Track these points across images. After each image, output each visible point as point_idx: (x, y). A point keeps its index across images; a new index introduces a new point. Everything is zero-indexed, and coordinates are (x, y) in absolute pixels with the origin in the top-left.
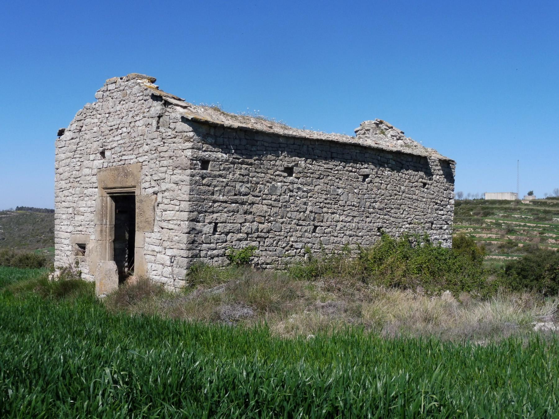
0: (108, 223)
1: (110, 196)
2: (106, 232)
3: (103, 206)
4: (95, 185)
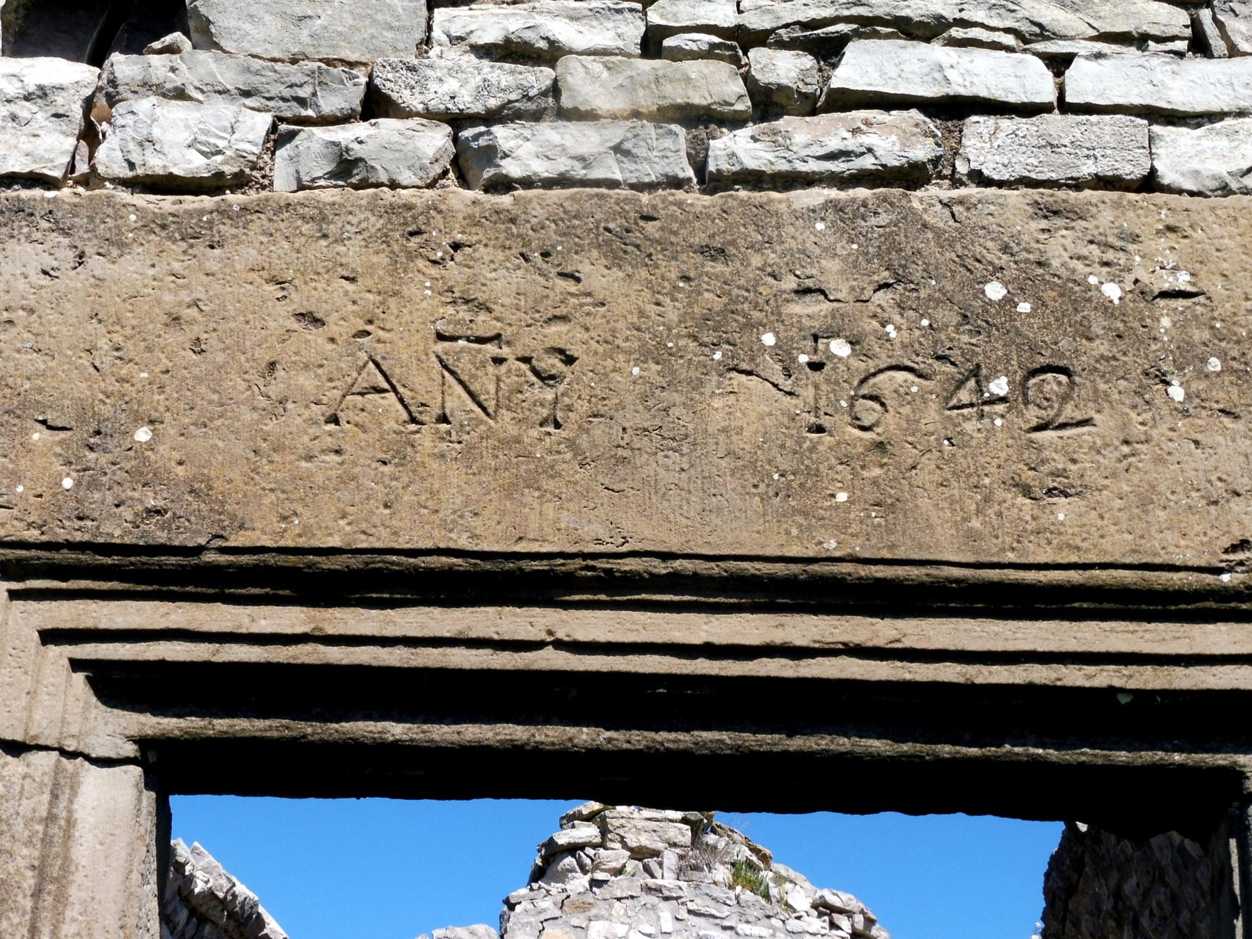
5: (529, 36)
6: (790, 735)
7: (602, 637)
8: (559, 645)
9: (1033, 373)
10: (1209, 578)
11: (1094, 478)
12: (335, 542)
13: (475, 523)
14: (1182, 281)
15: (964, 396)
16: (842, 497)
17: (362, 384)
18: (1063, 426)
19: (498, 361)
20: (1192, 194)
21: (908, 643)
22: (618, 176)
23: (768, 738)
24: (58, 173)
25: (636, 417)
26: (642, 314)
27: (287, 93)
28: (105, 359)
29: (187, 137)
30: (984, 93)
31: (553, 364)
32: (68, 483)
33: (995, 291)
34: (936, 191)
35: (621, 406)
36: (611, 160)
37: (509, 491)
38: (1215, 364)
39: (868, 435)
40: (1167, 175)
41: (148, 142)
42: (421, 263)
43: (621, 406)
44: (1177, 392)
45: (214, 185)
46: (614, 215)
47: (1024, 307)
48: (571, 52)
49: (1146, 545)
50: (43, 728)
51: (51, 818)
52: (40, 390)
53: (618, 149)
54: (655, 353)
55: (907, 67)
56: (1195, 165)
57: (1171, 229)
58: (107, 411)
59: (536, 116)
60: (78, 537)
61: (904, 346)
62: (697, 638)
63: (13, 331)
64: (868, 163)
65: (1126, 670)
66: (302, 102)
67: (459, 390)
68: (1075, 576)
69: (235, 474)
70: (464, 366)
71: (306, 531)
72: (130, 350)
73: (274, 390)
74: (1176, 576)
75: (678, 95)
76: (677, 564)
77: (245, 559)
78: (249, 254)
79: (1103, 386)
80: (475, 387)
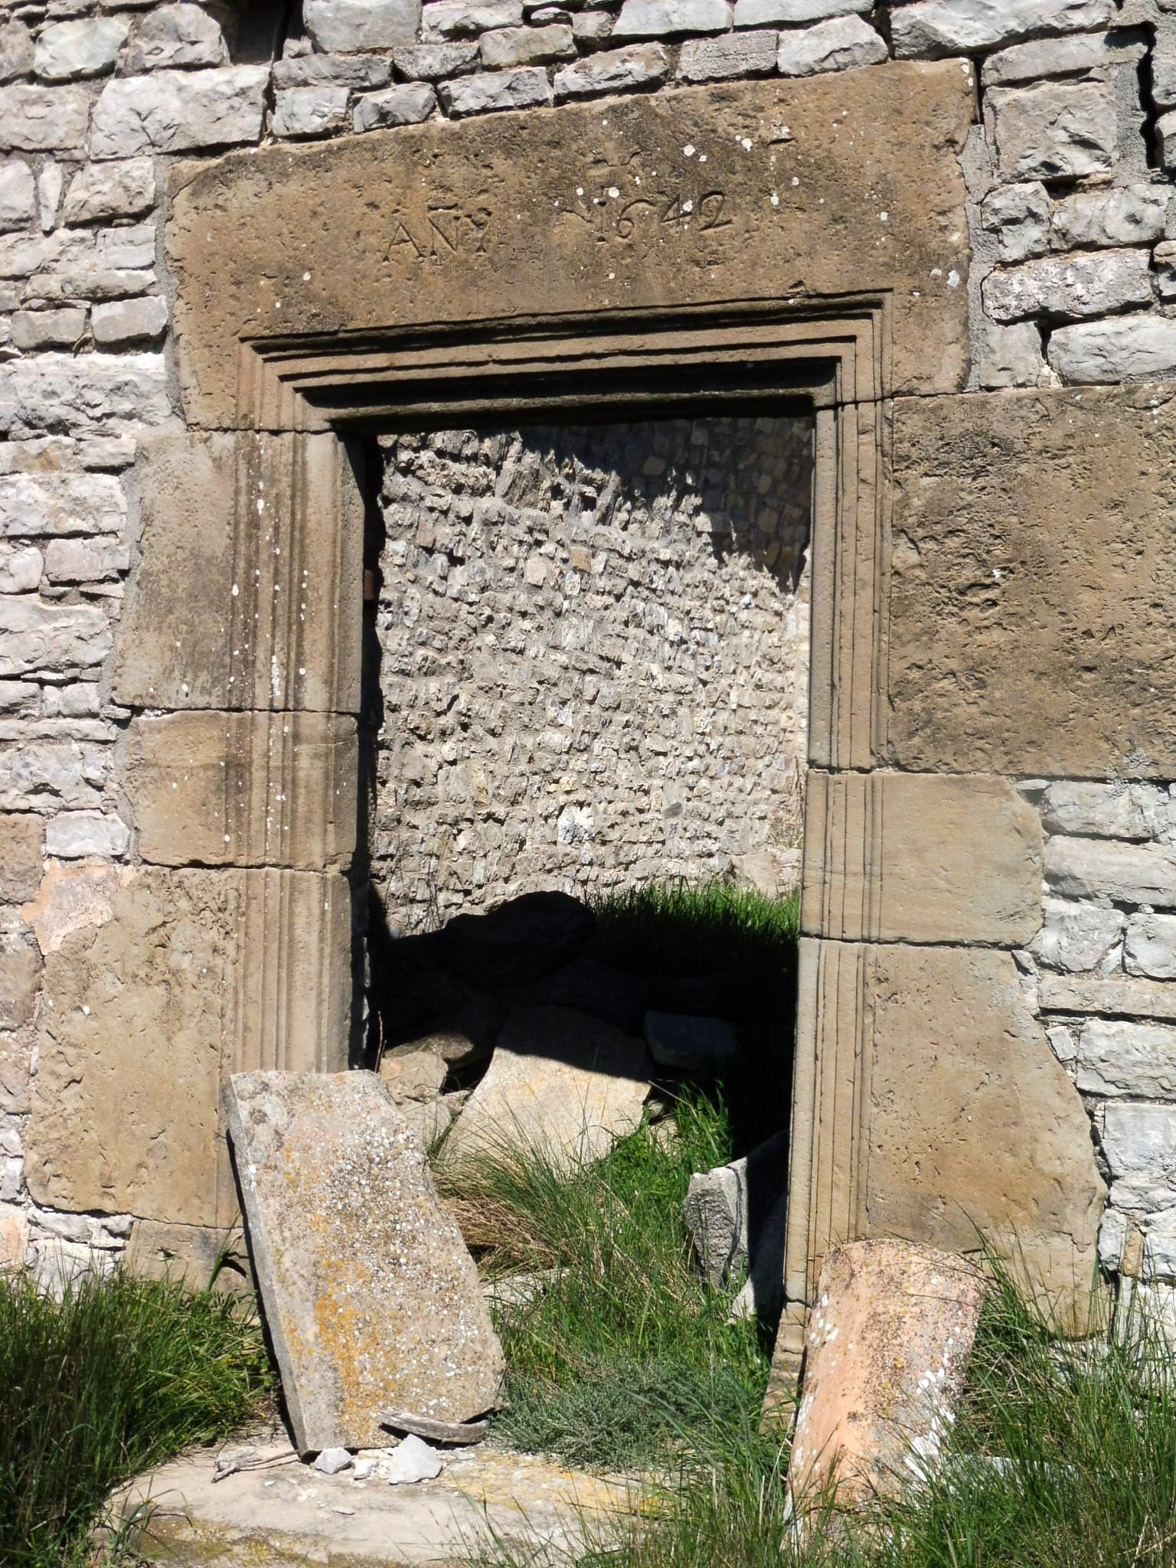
0: (315, 695)
1: (339, 427)
2: (291, 785)
3: (255, 523)
4: (147, 317)
5: (466, 22)
6: (604, 394)
7: (513, 356)
8: (495, 362)
9: (706, 196)
10: (782, 303)
11: (731, 253)
12: (391, 323)
13: (450, 306)
14: (784, 132)
15: (671, 214)
16: (612, 276)
17: (398, 238)
18: (718, 225)
19: (457, 218)
20: (797, 76)
21: (647, 347)
22: (511, 103)
23: (594, 396)
24: (255, 138)
25: (519, 243)
26: (521, 184)
27: (354, 75)
28: (287, 239)
29: (310, 109)
30: (690, 27)
31: (483, 216)
32: (278, 305)
33: (689, 150)
34: (667, 91)
35: (512, 237)
36: (507, 94)
37: (463, 289)
38: (796, 181)
39: (626, 241)
40: (784, 68)
41: (292, 115)
42: (420, 168)
43: (512, 237)
44: (775, 200)
45: (325, 135)
46: (506, 129)
47: (703, 158)
48: (488, 29)
49: (752, 288)
50: (286, 421)
51: (294, 463)
52: (261, 259)
53: (509, 88)
54: (526, 206)
55: (652, 17)
56: (797, 58)
57: (781, 100)
58: (290, 265)
59: (472, 71)
60: (286, 332)
61: (644, 188)
62: (553, 353)
63: (246, 229)
64: (629, 80)
65: (749, 352)
66: (363, 79)
67: (440, 237)
68: (718, 307)
69: (346, 292)
70: (441, 223)
71: (379, 318)
72: (298, 232)
73: (360, 247)
74: (766, 303)
75: (539, 50)
76: (539, 318)
77: (355, 334)
78: (343, 174)
79: (738, 201)
80: (447, 234)
